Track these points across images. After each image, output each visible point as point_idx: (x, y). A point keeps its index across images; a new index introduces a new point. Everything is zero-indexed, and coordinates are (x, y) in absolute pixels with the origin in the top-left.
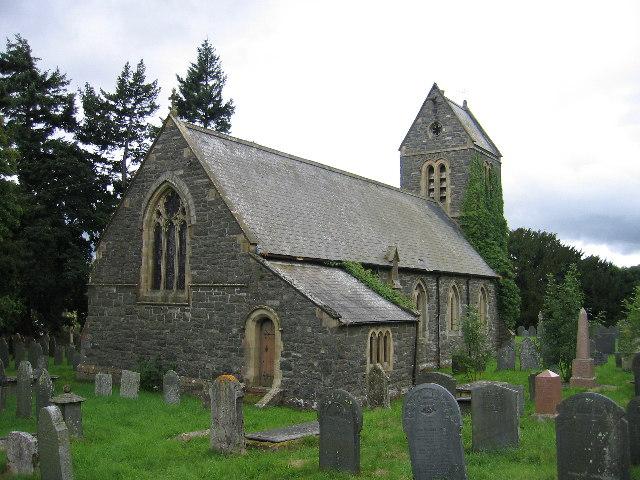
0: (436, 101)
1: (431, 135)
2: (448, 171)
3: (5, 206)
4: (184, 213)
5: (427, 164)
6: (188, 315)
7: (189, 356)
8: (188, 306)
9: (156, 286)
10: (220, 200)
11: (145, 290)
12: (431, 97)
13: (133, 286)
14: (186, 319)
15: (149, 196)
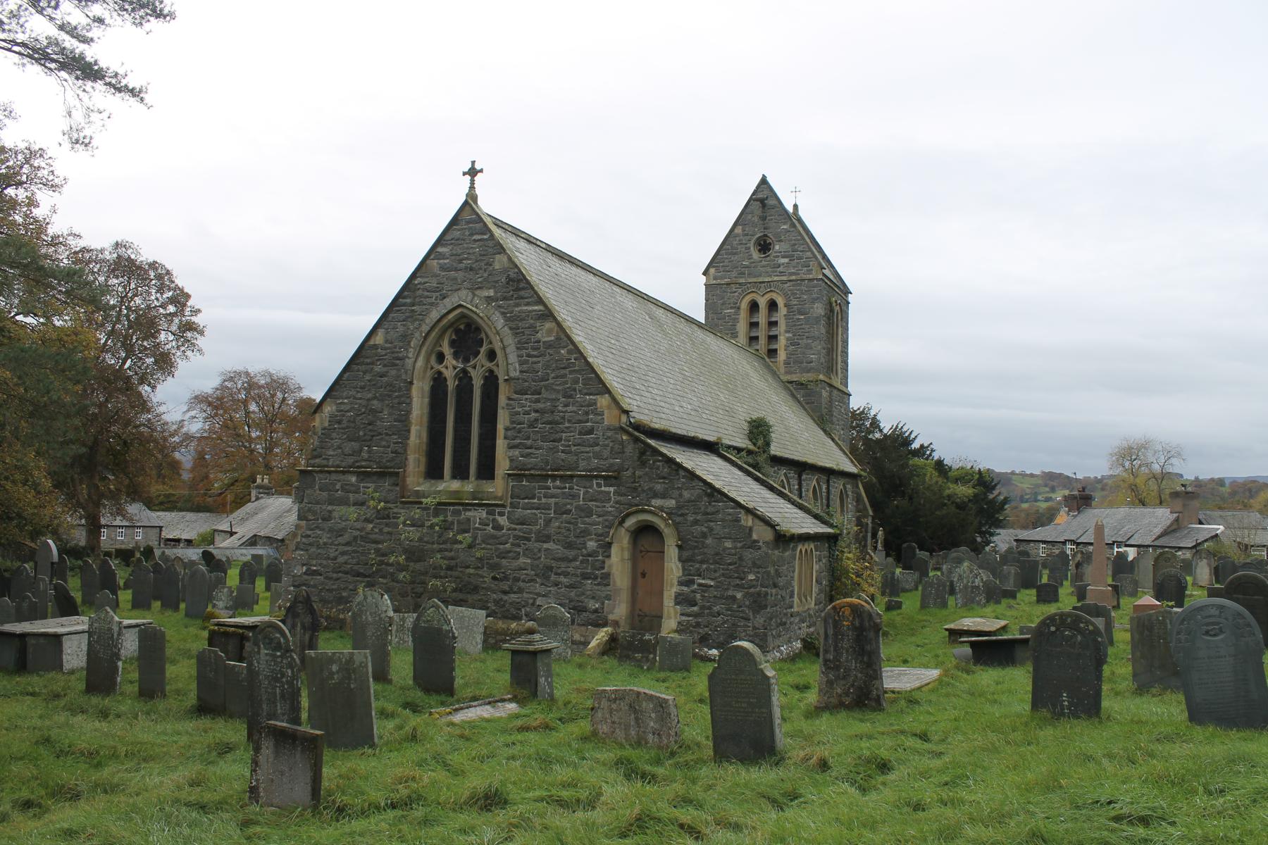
0: (763, 198)
1: (756, 255)
2: (782, 310)
3: (4, 336)
4: (492, 355)
5: (748, 298)
6: (502, 521)
7: (505, 586)
8: (503, 506)
9: (434, 471)
10: (564, 337)
11: (415, 480)
12: (760, 196)
13: (390, 473)
14: (498, 527)
15: (425, 328)
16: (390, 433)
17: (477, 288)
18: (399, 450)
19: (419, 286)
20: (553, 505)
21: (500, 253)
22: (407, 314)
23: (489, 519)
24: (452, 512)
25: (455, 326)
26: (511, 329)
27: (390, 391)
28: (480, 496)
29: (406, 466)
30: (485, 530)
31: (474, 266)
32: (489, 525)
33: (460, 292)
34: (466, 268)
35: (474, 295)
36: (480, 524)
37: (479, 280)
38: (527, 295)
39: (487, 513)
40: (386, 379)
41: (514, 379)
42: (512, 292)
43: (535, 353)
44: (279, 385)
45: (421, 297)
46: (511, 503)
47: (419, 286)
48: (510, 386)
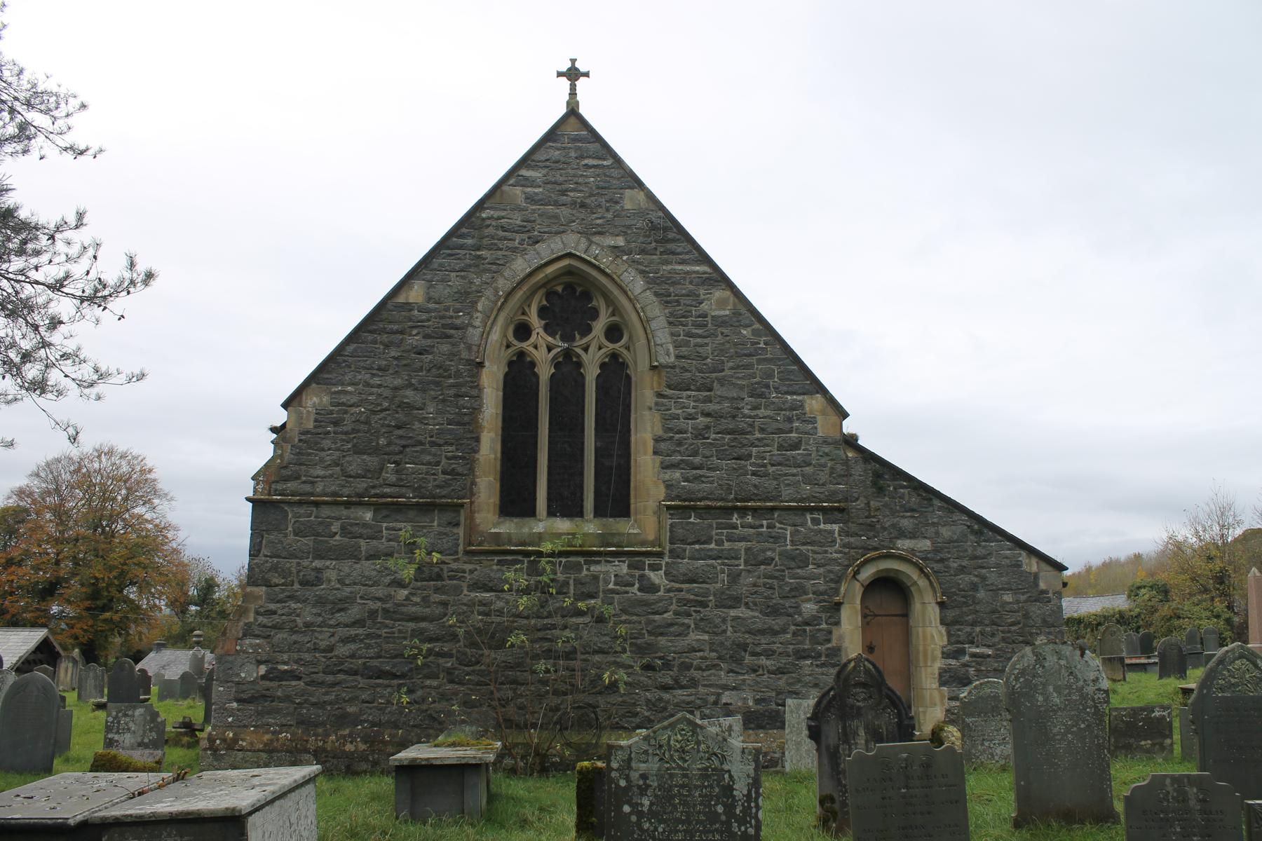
16: (441, 442)
17: (595, 233)
18: (460, 470)
23: (633, 576)
25: (549, 287)
26: (656, 294)
27: (440, 376)
28: (615, 540)
29: (472, 494)
30: (627, 592)
31: (587, 201)
32: (633, 585)
33: (564, 236)
34: (574, 203)
35: (591, 243)
36: (616, 584)
37: (599, 222)
38: (679, 250)
39: (629, 567)
41: (667, 367)
42: (654, 244)
43: (699, 331)
45: (493, 238)
46: (671, 551)
47: (488, 222)
48: (660, 377)
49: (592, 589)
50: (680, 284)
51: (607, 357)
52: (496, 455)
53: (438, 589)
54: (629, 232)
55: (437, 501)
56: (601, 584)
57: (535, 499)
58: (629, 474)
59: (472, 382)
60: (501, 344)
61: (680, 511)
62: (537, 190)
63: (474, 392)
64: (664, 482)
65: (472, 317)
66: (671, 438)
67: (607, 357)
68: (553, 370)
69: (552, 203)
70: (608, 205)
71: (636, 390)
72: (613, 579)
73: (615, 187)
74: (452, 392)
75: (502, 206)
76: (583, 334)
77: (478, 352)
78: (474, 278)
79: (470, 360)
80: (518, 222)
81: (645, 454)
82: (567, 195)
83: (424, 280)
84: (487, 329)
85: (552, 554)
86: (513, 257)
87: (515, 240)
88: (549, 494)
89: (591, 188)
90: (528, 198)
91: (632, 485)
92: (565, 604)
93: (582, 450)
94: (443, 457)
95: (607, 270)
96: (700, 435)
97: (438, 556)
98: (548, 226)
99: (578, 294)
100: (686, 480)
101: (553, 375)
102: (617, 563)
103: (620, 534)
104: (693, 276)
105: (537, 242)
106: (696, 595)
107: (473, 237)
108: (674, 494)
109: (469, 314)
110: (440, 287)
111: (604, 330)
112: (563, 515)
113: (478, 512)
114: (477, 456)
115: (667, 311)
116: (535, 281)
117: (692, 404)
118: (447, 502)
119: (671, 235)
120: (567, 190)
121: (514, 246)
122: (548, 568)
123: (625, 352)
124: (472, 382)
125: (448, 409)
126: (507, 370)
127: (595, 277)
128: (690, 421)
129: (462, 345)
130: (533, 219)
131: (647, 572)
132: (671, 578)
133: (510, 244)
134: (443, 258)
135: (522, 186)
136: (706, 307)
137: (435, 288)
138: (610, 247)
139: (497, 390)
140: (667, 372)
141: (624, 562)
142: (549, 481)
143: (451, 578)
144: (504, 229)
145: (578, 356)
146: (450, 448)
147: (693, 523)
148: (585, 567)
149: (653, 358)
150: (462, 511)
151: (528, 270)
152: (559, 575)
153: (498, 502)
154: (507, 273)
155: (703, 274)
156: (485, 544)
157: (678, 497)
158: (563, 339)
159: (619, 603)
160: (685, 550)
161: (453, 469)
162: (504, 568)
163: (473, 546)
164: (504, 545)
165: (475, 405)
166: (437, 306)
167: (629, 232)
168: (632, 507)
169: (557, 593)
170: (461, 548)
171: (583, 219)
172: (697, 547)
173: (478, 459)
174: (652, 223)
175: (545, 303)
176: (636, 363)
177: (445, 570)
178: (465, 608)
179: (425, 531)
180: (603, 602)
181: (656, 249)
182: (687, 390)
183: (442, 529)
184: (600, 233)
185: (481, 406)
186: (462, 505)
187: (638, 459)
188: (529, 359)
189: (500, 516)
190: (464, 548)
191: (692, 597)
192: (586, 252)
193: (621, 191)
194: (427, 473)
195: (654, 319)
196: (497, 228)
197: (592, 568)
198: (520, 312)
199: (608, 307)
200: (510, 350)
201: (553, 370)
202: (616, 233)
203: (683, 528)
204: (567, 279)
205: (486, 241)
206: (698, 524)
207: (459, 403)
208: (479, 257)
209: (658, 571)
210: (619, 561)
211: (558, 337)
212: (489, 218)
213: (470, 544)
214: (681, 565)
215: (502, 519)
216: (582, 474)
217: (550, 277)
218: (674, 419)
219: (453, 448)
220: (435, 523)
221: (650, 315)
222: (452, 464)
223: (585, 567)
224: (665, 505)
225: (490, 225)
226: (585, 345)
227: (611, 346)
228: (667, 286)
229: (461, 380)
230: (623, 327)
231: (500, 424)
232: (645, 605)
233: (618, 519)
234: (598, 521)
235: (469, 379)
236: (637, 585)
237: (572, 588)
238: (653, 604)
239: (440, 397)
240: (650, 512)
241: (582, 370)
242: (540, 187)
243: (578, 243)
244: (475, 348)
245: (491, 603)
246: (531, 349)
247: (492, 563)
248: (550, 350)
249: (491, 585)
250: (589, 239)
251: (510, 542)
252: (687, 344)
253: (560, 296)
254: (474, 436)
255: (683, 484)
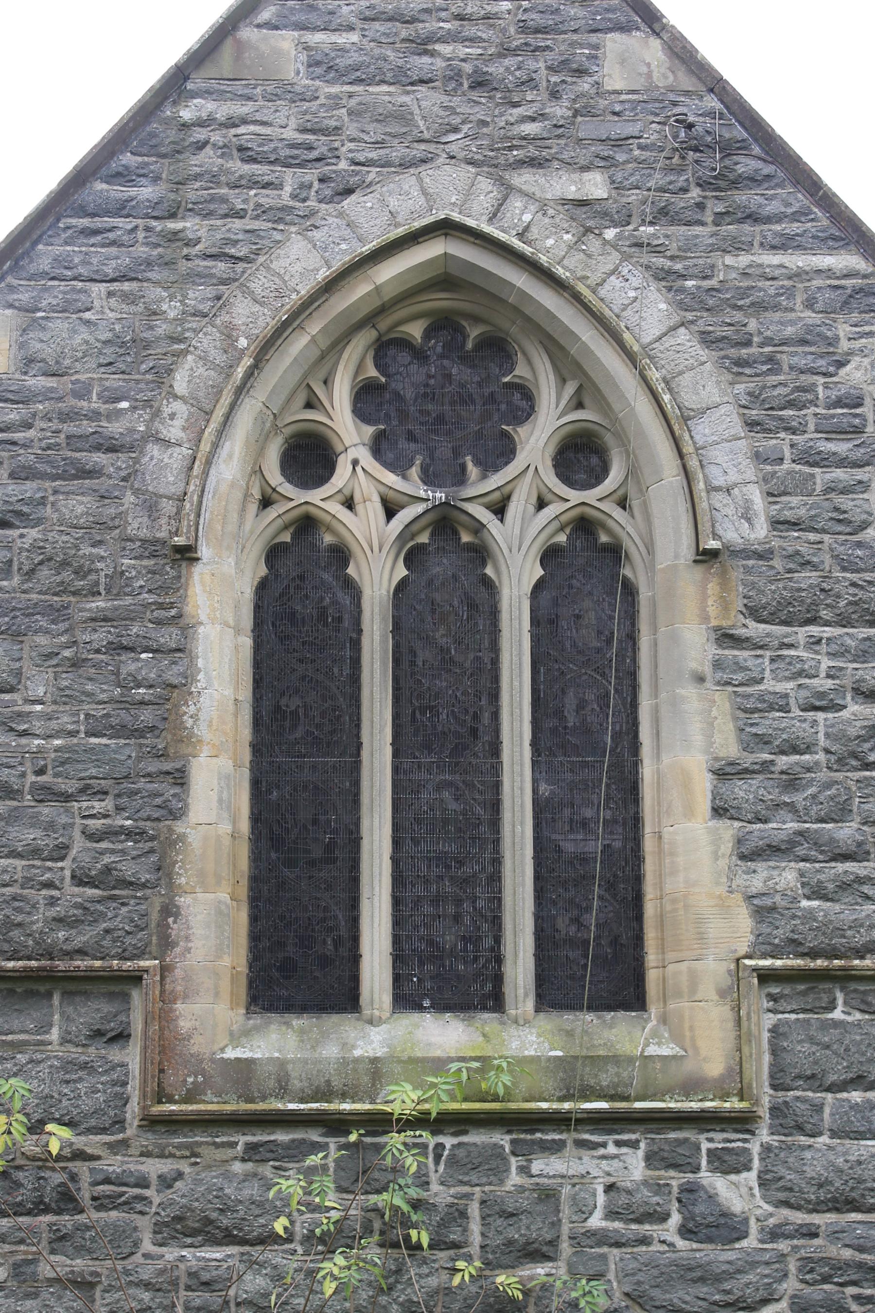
16: (70, 786)
17: (521, 163)
18: (128, 869)
19: (200, 134)
20: (704, 1162)
21: (623, 28)
22: (141, 251)
23: (660, 1188)
24: (453, 1161)
25: (384, 324)
26: (707, 340)
27: (63, 589)
28: (605, 1079)
29: (166, 943)
30: (645, 1241)
31: (495, 69)
32: (664, 1218)
33: (427, 173)
34: (454, 76)
35: (508, 190)
36: (611, 1214)
37: (530, 128)
38: (773, 208)
39: (650, 1159)
40: (33, 533)
41: (746, 553)
42: (695, 193)
43: (841, 448)
44: (697, 51)
45: (214, 179)
46: (775, 1110)
47: (200, 134)
48: (724, 583)
49: (90, 305)
50: (776, 307)
51: (562, 529)
52: (234, 823)
53: (63, 1238)
54: (621, 157)
55: (61, 965)
56: (566, 1212)
57: (356, 958)
58: (638, 879)
59: (161, 606)
60: (247, 495)
61: (801, 987)
62: (342, 39)
63: (168, 637)
64: (750, 898)
65: (157, 413)
66: (766, 767)
67: (562, 529)
68: (402, 571)
69: (389, 76)
70: (554, 79)
71: (655, 630)
72: (601, 1199)
73: (574, 25)
74: (101, 636)
75: (239, 88)
76: (489, 466)
77: (178, 515)
78: (162, 300)
79: (157, 541)
80: (290, 134)
81: (689, 812)
82: (432, 54)
83: (11, 306)
84: (205, 446)
85: (421, 1121)
86: (277, 236)
87: (280, 187)
88: (397, 940)
89: (504, 31)
90: (318, 64)
91: (650, 909)
92: (457, 1280)
93: (496, 806)
94: (77, 834)
95: (560, 271)
96: (854, 755)
97: (65, 1133)
98: (379, 144)
99: (470, 345)
100: (818, 893)
101: (402, 585)
102: (612, 1149)
103: (615, 1059)
104: (817, 282)
105: (349, 191)
106: (861, 1249)
107: (156, 179)
108: (781, 934)
109: (148, 403)
110: (59, 326)
111: (551, 450)
112: (442, 1006)
113: (186, 997)
114: (180, 827)
115: (740, 388)
116: (340, 308)
117: (826, 663)
118: (92, 969)
119: (745, 165)
120: (431, 39)
121: (279, 203)
122: (411, 1163)
123: (617, 513)
124: (161, 606)
125: (89, 687)
126: (263, 571)
127: (523, 294)
128: (820, 716)
129: (129, 498)
130: (333, 123)
131: (706, 1177)
132: (782, 1196)
133: (267, 198)
134: (66, 243)
135: (303, 27)
136: (858, 375)
137: (44, 329)
138: (564, 202)
139: (238, 631)
140: (748, 570)
141: (634, 1145)
142: (398, 880)
143: (100, 1203)
144: (246, 154)
145: (478, 528)
146: (98, 806)
147: (836, 1024)
148: (514, 1162)
149: (705, 527)
150: (136, 996)
151: (323, 274)
152: (435, 1187)
153: (243, 968)
154: (260, 283)
155: (846, 276)
156: (209, 1096)
157: (794, 946)
158: (429, 478)
159: (625, 1274)
160: (818, 1108)
161: (108, 870)
162: (267, 1170)
163: (171, 1101)
164: (264, 1098)
165: (172, 675)
166: (51, 382)
167: (621, 157)
168: (652, 976)
169: (431, 1247)
170: (133, 1110)
171: (484, 123)
172: (856, 1096)
173: (182, 838)
174: (690, 126)
175: (372, 372)
176: (650, 548)
177: (86, 1178)
178: (146, 1296)
179: (22, 1058)
180: (573, 1272)
181: (701, 206)
182: (812, 621)
183: (74, 1052)
184: (533, 163)
185: (189, 677)
186: (136, 978)
187: (667, 831)
188: (328, 539)
189: (248, 1011)
190: (144, 1108)
191: (847, 1254)
192: (492, 218)
193: (594, 38)
194: (27, 883)
195: (703, 412)
196: (224, 150)
197: (537, 1166)
198: (301, 398)
199: (562, 380)
200: (273, 513)
201: (402, 571)
202: (582, 162)
203: (812, 1040)
204: (440, 301)
205: (193, 193)
206: (858, 1025)
207: (124, 671)
208: (174, 237)
209: (738, 1171)
210: (618, 1144)
211: (414, 472)
212: (201, 123)
213: (161, 1096)
214: (808, 1155)
215: (256, 1020)
216: (495, 878)
217: (388, 294)
218: (771, 708)
219: (108, 804)
220: (55, 1035)
221: (690, 400)
222: (102, 853)
223: (514, 1162)
224: (755, 969)
225: (206, 143)
226: (497, 495)
227: (575, 496)
228: (738, 316)
229: (128, 600)
230: (609, 439)
231: (246, 733)
232: (702, 1280)
233: (609, 1016)
234: (548, 1022)
235: (151, 598)
236: (675, 1219)
237: (475, 1227)
238: (729, 1276)
239: (67, 653)
240: (708, 990)
241: (489, 571)
242: (351, 28)
243: (468, 193)
244: (168, 507)
245: (227, 1282)
246: (336, 508)
247: (230, 1153)
248: (390, 512)
249: (225, 1222)
250: (501, 182)
251: (283, 1090)
252: (804, 486)
253: (419, 354)
254: (168, 766)
255: (805, 903)
